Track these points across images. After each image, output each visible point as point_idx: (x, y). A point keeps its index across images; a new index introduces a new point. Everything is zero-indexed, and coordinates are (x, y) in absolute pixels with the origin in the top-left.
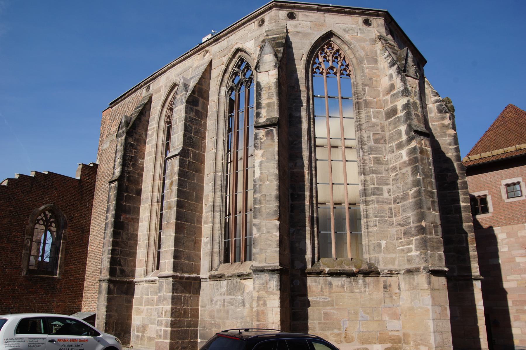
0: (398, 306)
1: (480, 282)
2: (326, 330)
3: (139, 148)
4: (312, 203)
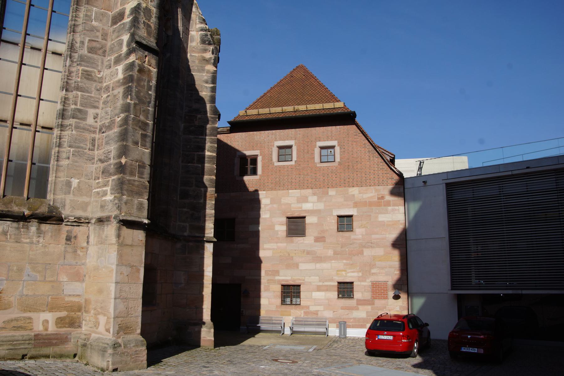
0: (83, 264)
1: (212, 244)
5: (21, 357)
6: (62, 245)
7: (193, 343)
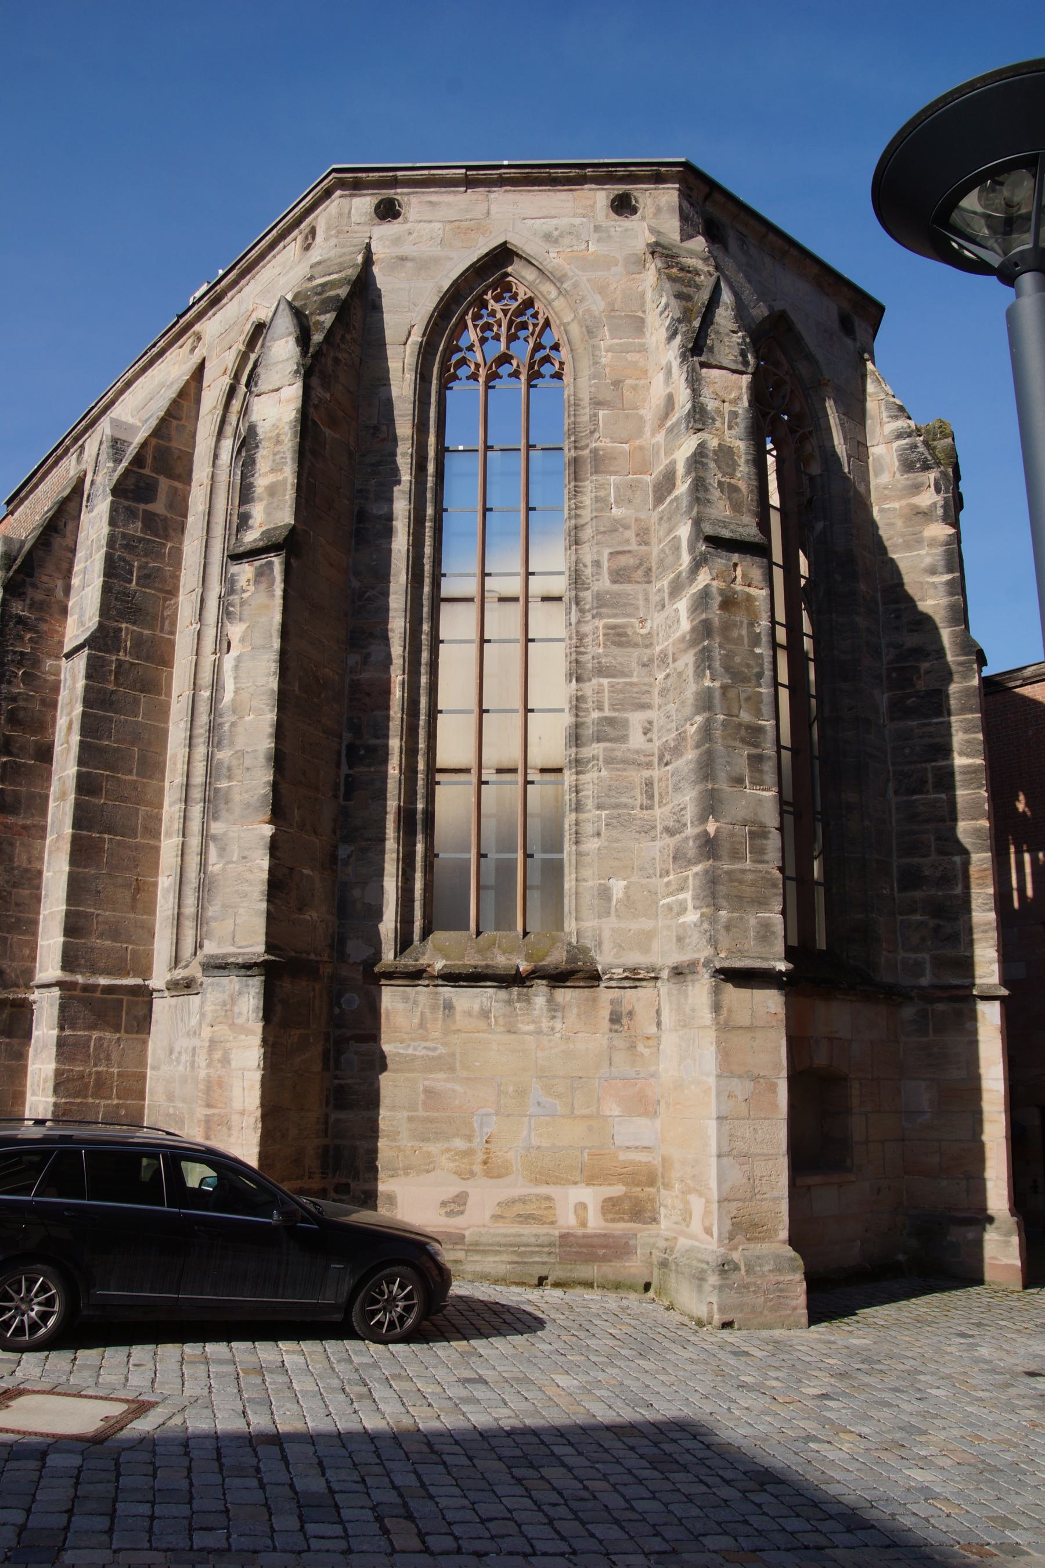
0: (652, 1076)
1: (996, 1005)
2: (429, 1140)
3: (44, 627)
4: (409, 771)
5: (536, 1282)
6: (603, 1034)
7: (964, 1272)
